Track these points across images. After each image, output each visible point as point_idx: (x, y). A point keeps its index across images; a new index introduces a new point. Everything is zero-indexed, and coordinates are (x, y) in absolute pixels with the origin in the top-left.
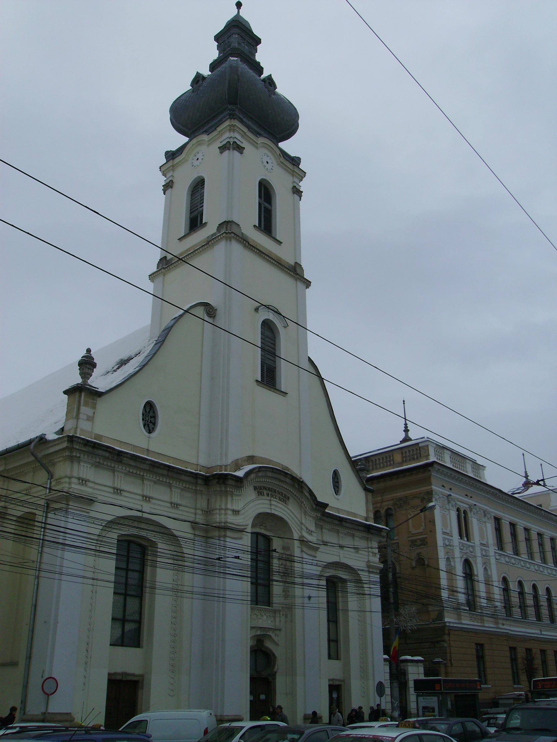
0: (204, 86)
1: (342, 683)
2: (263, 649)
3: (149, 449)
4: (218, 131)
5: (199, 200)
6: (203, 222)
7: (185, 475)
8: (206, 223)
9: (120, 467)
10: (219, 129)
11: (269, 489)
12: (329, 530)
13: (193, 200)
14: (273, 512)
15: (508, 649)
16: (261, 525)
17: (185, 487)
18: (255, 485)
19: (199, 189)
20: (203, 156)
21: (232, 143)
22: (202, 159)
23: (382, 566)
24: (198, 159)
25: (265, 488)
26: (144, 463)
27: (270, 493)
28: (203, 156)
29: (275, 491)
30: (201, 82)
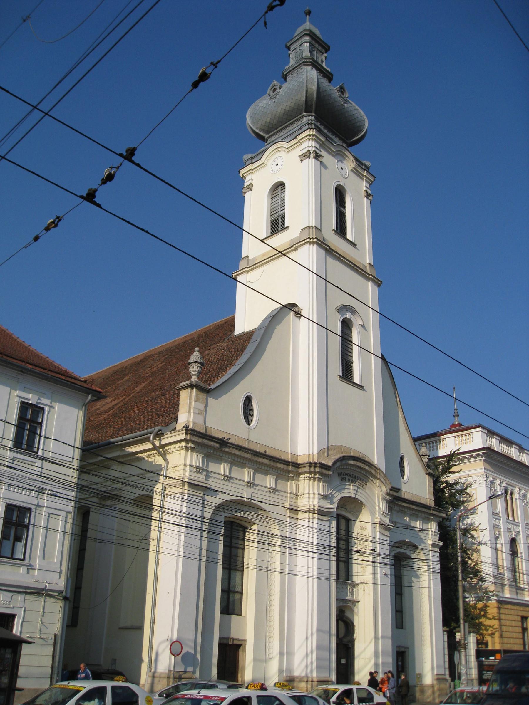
0: (282, 94)
1: (406, 650)
2: (344, 618)
3: (250, 439)
4: (298, 139)
5: (280, 203)
6: (286, 226)
7: (281, 463)
8: (288, 227)
9: (227, 456)
10: (299, 138)
11: (351, 475)
12: (398, 512)
13: (273, 204)
14: (357, 497)
15: (519, 618)
16: (342, 507)
17: (258, 467)
18: (339, 472)
19: (279, 193)
20: (283, 162)
21: (311, 152)
22: (282, 165)
23: (442, 544)
24: (277, 165)
25: (347, 474)
26: (247, 452)
27: (351, 478)
28: (283, 162)
29: (355, 477)
30: (278, 90)
